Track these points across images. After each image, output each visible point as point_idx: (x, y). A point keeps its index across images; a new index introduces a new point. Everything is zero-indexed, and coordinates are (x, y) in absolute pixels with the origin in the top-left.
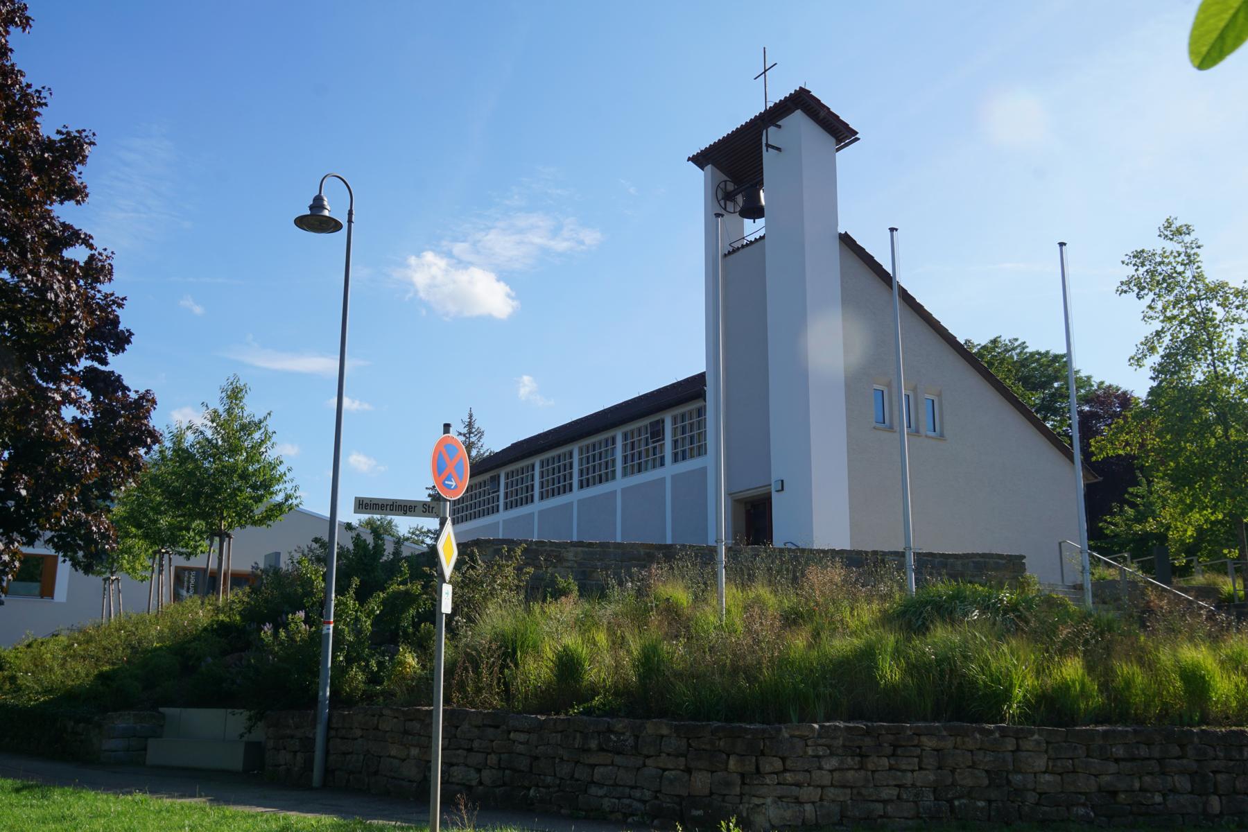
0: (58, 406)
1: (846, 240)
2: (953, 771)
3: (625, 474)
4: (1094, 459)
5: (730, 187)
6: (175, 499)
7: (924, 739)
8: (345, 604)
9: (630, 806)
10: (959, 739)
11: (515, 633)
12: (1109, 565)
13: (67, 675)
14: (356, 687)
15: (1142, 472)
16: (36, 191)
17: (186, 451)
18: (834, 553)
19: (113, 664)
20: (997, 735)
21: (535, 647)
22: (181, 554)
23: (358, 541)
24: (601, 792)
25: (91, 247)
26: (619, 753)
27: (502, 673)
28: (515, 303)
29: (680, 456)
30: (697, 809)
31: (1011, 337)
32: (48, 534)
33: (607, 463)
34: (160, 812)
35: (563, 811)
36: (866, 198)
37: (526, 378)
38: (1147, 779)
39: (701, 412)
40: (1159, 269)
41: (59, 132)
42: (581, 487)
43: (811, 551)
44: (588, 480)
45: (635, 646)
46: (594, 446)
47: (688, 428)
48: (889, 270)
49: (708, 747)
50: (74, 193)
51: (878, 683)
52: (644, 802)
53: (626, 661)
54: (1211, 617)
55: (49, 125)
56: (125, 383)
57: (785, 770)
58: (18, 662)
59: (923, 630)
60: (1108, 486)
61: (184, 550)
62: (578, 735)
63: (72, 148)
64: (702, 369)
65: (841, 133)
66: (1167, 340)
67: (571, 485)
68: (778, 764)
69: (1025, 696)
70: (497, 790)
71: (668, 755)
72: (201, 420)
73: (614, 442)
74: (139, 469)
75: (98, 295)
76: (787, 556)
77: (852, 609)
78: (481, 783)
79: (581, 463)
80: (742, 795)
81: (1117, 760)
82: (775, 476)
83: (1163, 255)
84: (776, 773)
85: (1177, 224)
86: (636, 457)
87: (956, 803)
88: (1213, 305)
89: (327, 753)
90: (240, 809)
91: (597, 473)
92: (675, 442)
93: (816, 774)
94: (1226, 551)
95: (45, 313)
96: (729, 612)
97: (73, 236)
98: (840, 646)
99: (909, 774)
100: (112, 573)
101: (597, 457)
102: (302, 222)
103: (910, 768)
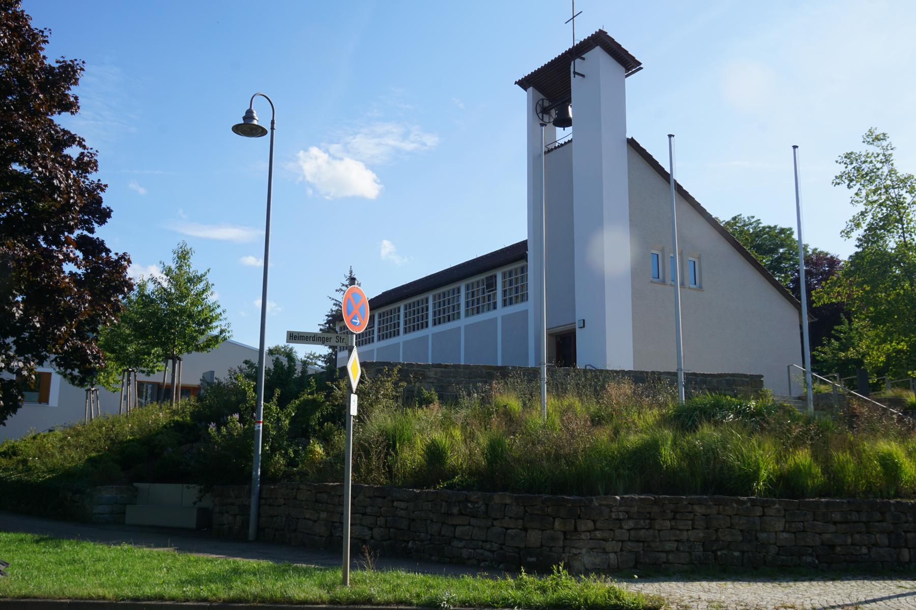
0: (60, 262)
1: (632, 143)
2: (717, 530)
3: (467, 315)
4: (814, 305)
5: (547, 103)
6: (140, 331)
7: (696, 507)
8: (270, 409)
9: (482, 554)
10: (721, 507)
11: (395, 429)
12: (825, 383)
13: (65, 459)
14: (279, 469)
15: (845, 314)
16: (40, 105)
17: (148, 296)
18: (624, 373)
19: (98, 451)
20: (749, 504)
21: (409, 440)
22: (143, 372)
23: (277, 363)
24: (461, 545)
25: (84, 147)
26: (474, 517)
27: (386, 458)
28: (381, 186)
29: (508, 302)
30: (531, 557)
31: (750, 215)
32: (53, 356)
33: (454, 307)
34: (143, 557)
35: (433, 558)
36: (648, 111)
37: (385, 242)
38: (857, 536)
39: (524, 270)
40: (864, 166)
41: (57, 62)
42: (435, 324)
43: (607, 371)
44: (439, 319)
45: (483, 440)
46: (444, 294)
47: (514, 282)
48: (668, 170)
49: (539, 512)
50: (69, 106)
51: (661, 467)
52: (493, 552)
53: (477, 451)
54: (900, 420)
55: (52, 55)
56: (107, 246)
57: (596, 529)
58: (27, 450)
59: (693, 428)
60: (824, 324)
61: (145, 369)
62: (444, 504)
63: (68, 73)
64: (525, 238)
65: (629, 63)
66: (869, 218)
67: (427, 323)
68: (590, 525)
69: (768, 476)
70: (384, 543)
71: (510, 518)
72: (156, 272)
73: (459, 291)
74: (119, 310)
75: (87, 182)
76: (589, 375)
77: (639, 413)
78: (372, 538)
79: (434, 306)
80: (564, 547)
81: (835, 523)
82: (579, 316)
83: (867, 156)
84: (589, 531)
85: (877, 132)
86: (476, 302)
87: (719, 553)
88: (903, 192)
89: (259, 515)
90: (201, 556)
91: (446, 314)
92: (505, 292)
93: (618, 532)
94: (910, 373)
95: (51, 195)
96: (550, 414)
97: (71, 139)
98: (633, 440)
99: (685, 533)
100: (92, 386)
101: (446, 302)
102: (237, 129)
103: (686, 528)
